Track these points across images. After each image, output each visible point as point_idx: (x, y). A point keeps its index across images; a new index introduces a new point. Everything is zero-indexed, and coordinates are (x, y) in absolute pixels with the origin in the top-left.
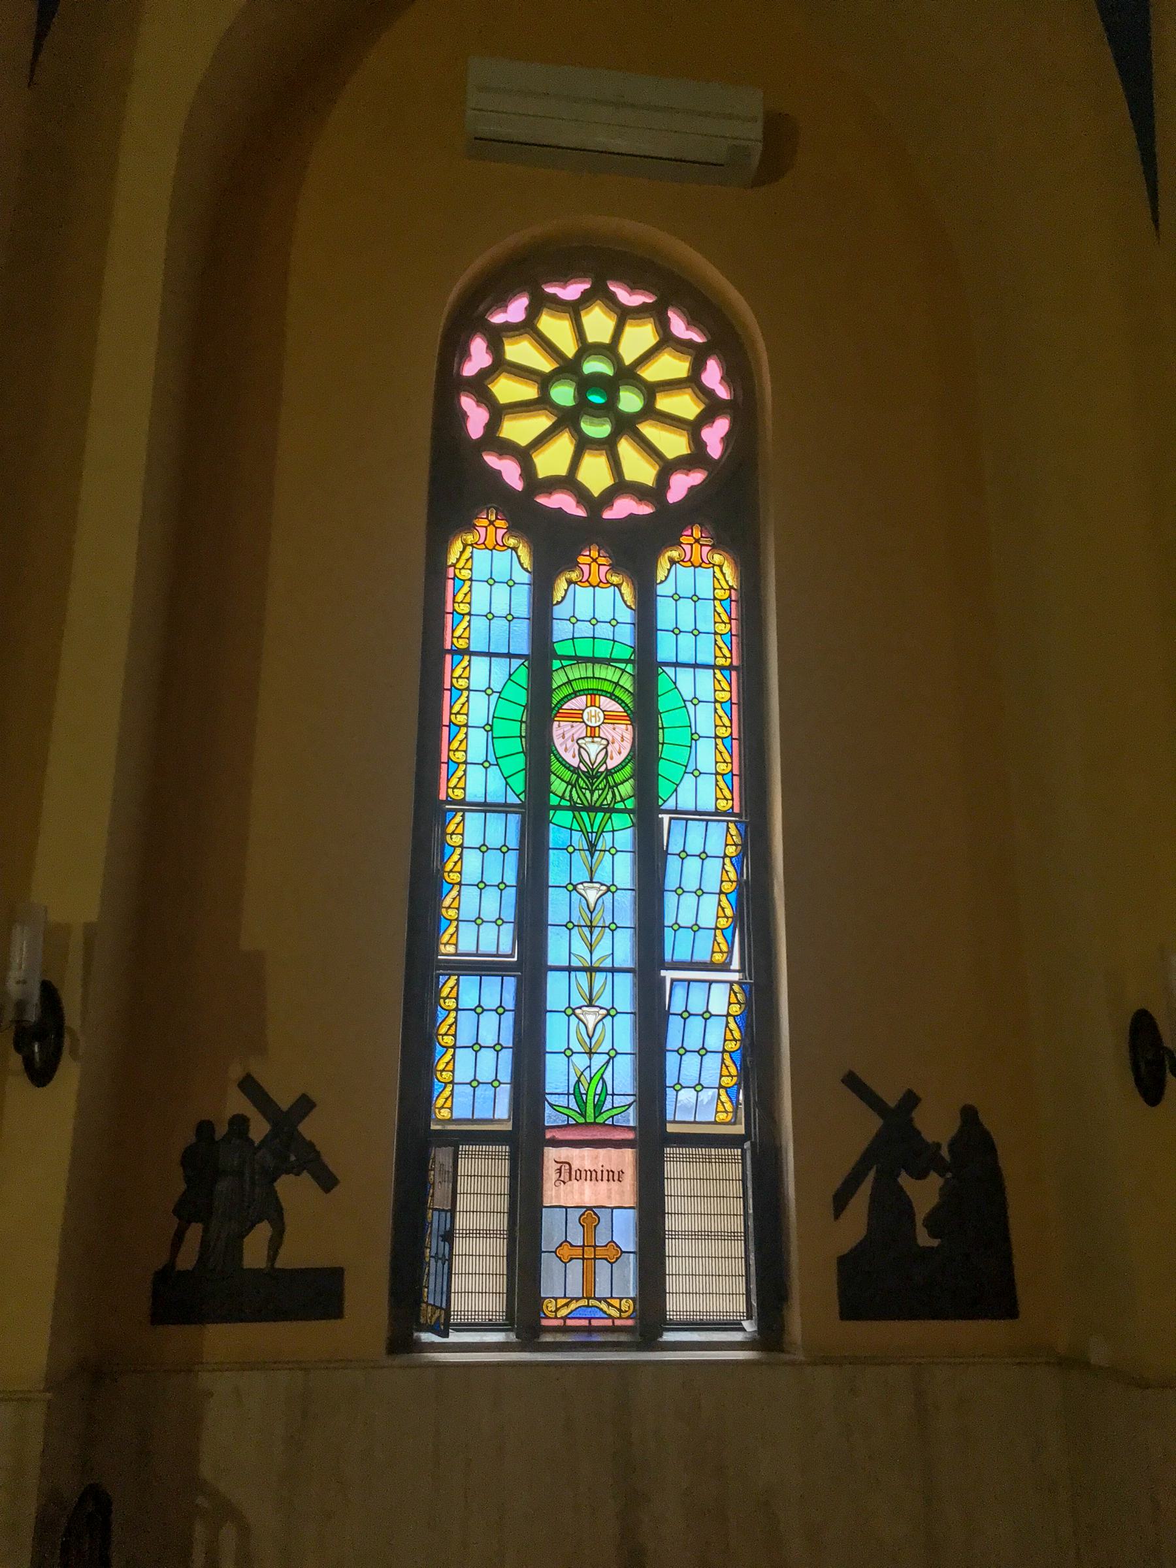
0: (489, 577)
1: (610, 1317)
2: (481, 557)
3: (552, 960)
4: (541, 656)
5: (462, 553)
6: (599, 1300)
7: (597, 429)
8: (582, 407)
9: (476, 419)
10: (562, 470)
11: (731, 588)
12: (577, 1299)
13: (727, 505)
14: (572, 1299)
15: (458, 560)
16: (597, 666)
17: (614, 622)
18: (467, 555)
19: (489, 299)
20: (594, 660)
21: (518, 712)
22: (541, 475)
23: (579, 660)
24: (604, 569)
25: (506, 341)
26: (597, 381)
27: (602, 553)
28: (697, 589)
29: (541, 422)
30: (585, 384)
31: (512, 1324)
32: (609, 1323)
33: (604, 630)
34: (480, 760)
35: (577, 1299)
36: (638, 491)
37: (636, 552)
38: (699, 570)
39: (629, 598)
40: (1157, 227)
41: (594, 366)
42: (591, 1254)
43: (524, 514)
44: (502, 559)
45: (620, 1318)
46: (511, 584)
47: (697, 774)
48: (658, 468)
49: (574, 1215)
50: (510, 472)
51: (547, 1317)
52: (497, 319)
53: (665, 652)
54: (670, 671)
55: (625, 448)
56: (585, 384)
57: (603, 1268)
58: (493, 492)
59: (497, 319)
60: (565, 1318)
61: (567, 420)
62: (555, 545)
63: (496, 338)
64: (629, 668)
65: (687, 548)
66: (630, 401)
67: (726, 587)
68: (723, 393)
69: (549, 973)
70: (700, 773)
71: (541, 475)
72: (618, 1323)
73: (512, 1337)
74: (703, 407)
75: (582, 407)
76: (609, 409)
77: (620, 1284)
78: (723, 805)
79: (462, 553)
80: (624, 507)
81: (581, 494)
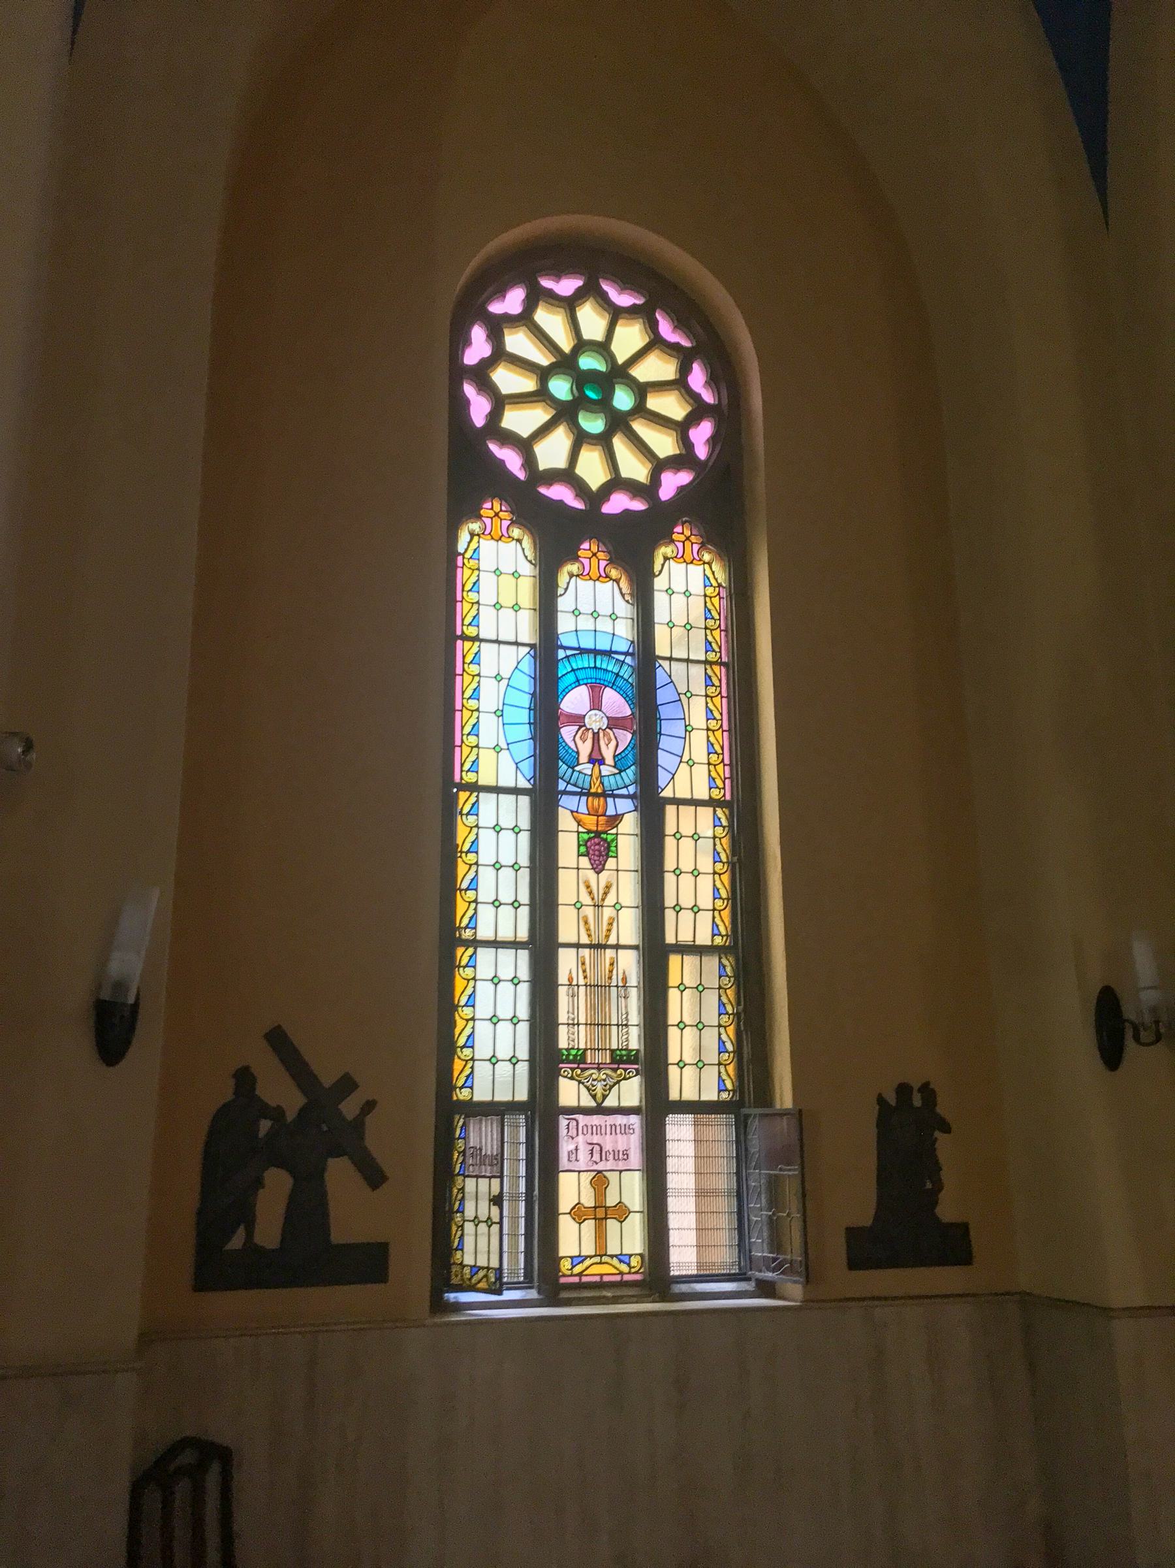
0: (496, 566)
1: (621, 1273)
2: (487, 546)
3: (562, 938)
4: (546, 648)
5: (469, 543)
6: (612, 1256)
7: (593, 424)
8: (579, 403)
9: (479, 409)
10: (561, 463)
11: (720, 585)
12: (591, 1257)
13: (716, 505)
14: (586, 1257)
15: (466, 550)
16: (599, 658)
17: (613, 617)
18: (474, 545)
19: (491, 289)
20: (596, 652)
21: (525, 700)
22: (542, 467)
23: (582, 651)
24: (603, 564)
25: (506, 331)
26: (593, 375)
27: (602, 548)
28: (687, 583)
29: (538, 415)
30: (582, 379)
31: (531, 1281)
32: (618, 1278)
33: (604, 625)
34: (493, 741)
35: (591, 1257)
36: (633, 488)
37: (631, 552)
38: (690, 566)
39: (626, 590)
40: (1099, 172)
41: (588, 362)
42: (602, 1213)
43: (528, 504)
44: (509, 550)
45: (629, 1273)
46: (516, 575)
47: (691, 764)
48: (650, 466)
49: (586, 1178)
50: (512, 460)
51: (564, 1276)
52: (546, 283)
53: (661, 649)
54: (665, 664)
55: (619, 444)
56: (582, 379)
57: (612, 1224)
58: (496, 481)
59: (546, 283)
60: (580, 1274)
61: (565, 413)
62: (558, 536)
63: (496, 327)
64: (629, 660)
65: (680, 545)
66: (623, 400)
67: (715, 584)
68: (708, 397)
69: (561, 950)
70: (693, 764)
71: (542, 467)
72: (627, 1278)
73: (533, 1294)
74: (689, 409)
75: (579, 403)
76: (604, 405)
77: (631, 1238)
78: (716, 794)
79: (469, 543)
80: (618, 503)
81: (580, 487)
